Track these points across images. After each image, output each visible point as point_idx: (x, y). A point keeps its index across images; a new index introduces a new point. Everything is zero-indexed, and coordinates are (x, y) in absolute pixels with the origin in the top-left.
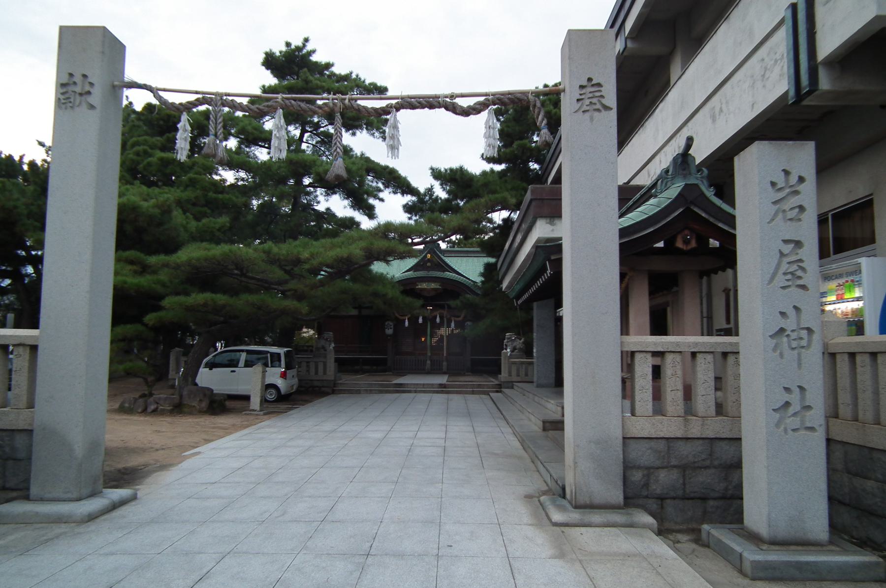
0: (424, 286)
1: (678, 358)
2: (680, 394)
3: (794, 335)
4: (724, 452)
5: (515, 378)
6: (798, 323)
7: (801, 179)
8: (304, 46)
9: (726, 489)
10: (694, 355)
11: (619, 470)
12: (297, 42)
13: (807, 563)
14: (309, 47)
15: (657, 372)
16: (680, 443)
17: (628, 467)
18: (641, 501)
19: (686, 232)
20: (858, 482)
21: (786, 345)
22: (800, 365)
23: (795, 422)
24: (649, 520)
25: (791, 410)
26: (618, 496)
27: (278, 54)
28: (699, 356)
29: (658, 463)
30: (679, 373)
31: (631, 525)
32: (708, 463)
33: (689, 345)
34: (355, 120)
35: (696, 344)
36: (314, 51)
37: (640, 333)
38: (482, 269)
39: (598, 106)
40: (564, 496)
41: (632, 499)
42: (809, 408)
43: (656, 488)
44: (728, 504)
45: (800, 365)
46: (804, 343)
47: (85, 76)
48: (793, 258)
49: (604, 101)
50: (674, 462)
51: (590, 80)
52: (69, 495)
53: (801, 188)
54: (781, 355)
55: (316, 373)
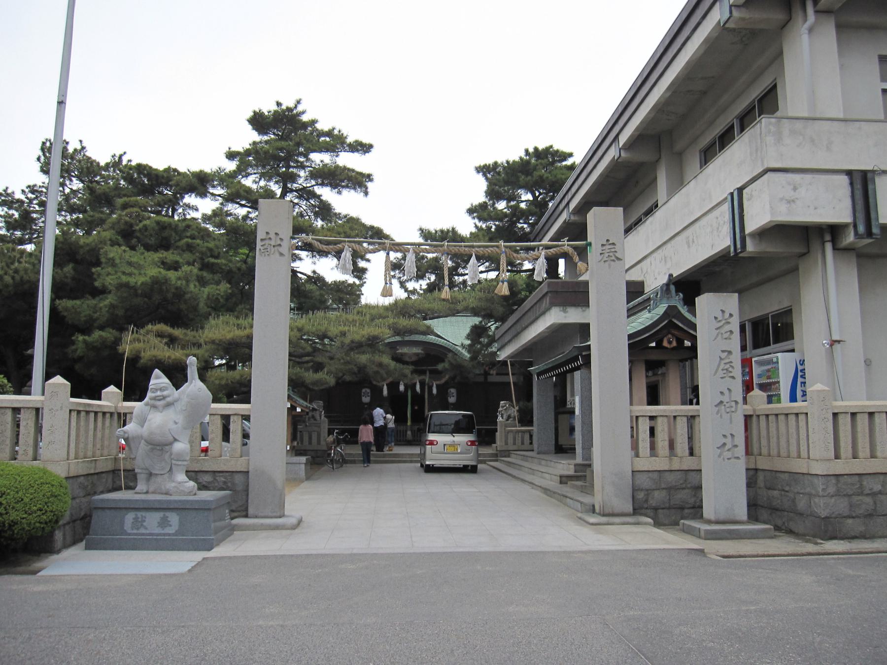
0: (405, 350)
1: (665, 419)
2: (667, 443)
3: (728, 405)
4: (692, 476)
5: (511, 447)
6: (730, 398)
7: (731, 315)
8: (296, 107)
9: (695, 502)
10: (675, 417)
11: (629, 492)
12: (288, 103)
13: (733, 530)
14: (300, 108)
15: (652, 431)
16: (667, 474)
17: (635, 489)
18: (643, 511)
19: (670, 336)
20: (771, 492)
21: (723, 411)
22: (731, 422)
23: (728, 454)
24: (650, 520)
25: (727, 447)
26: (629, 508)
27: (266, 114)
28: (678, 418)
29: (654, 487)
30: (666, 429)
31: (638, 524)
32: (684, 486)
33: (672, 411)
34: (338, 178)
35: (676, 411)
36: (303, 112)
37: (640, 404)
38: (468, 331)
39: (613, 258)
40: (594, 511)
41: (637, 510)
42: (736, 446)
43: (653, 503)
44: (696, 510)
45: (731, 422)
46: (733, 409)
47: (276, 234)
48: (727, 361)
49: (617, 255)
50: (663, 486)
51: (608, 240)
52: (275, 514)
53: (730, 320)
54: (721, 416)
55: (310, 443)
